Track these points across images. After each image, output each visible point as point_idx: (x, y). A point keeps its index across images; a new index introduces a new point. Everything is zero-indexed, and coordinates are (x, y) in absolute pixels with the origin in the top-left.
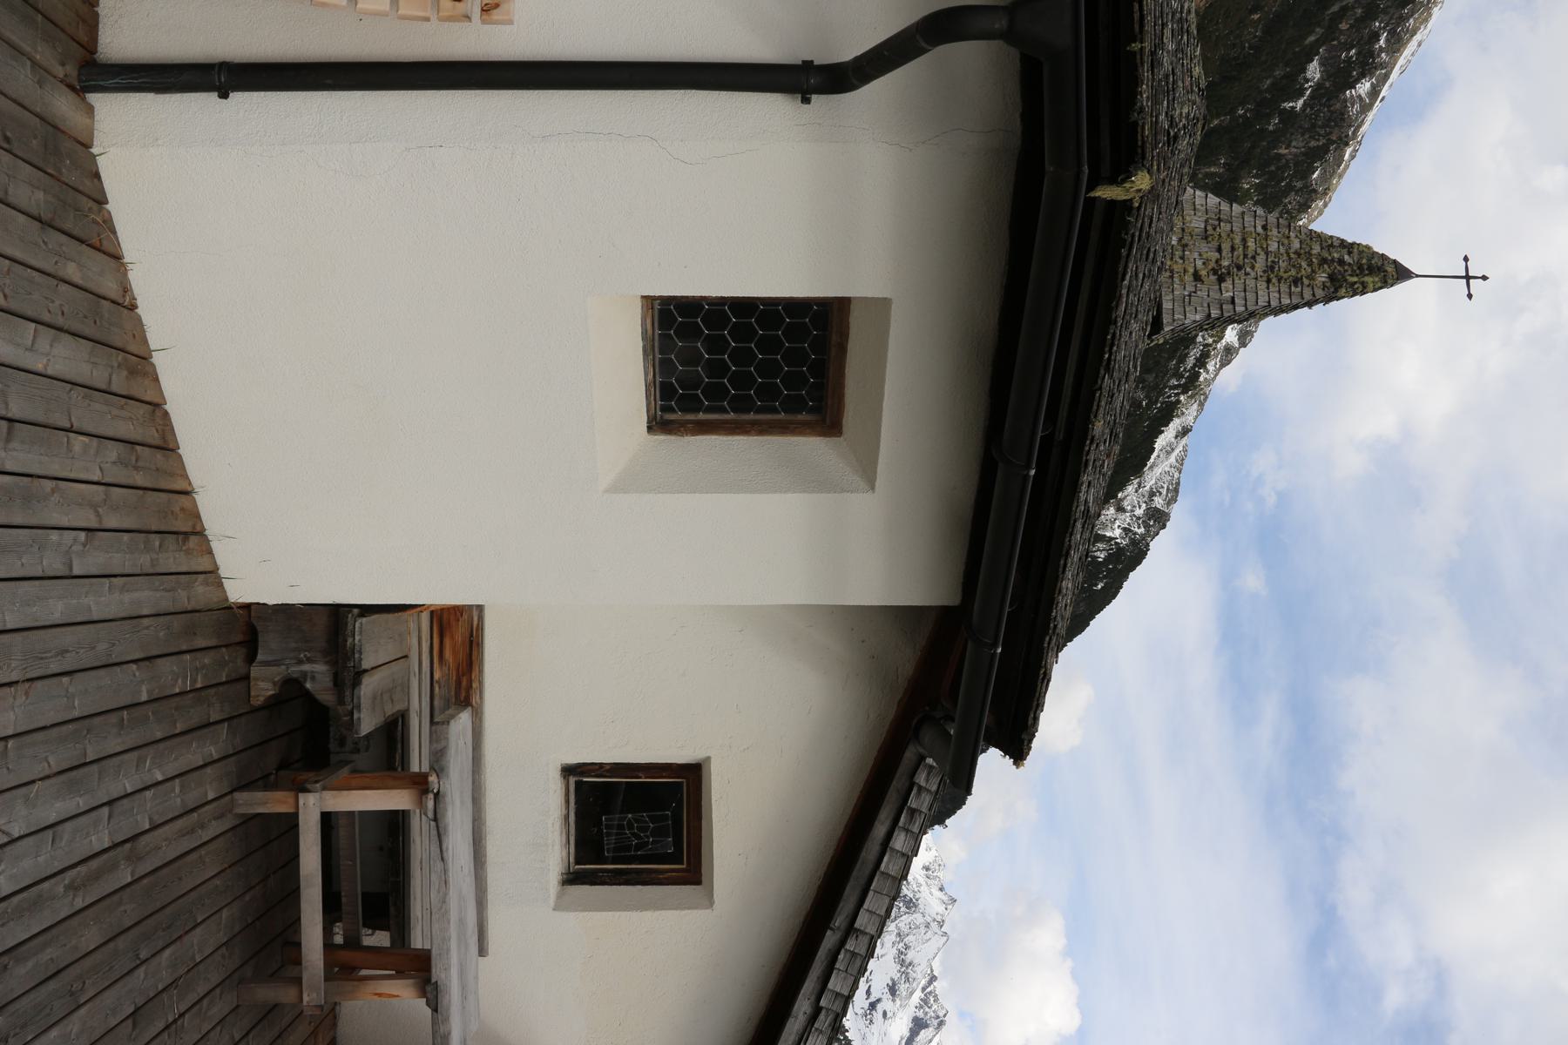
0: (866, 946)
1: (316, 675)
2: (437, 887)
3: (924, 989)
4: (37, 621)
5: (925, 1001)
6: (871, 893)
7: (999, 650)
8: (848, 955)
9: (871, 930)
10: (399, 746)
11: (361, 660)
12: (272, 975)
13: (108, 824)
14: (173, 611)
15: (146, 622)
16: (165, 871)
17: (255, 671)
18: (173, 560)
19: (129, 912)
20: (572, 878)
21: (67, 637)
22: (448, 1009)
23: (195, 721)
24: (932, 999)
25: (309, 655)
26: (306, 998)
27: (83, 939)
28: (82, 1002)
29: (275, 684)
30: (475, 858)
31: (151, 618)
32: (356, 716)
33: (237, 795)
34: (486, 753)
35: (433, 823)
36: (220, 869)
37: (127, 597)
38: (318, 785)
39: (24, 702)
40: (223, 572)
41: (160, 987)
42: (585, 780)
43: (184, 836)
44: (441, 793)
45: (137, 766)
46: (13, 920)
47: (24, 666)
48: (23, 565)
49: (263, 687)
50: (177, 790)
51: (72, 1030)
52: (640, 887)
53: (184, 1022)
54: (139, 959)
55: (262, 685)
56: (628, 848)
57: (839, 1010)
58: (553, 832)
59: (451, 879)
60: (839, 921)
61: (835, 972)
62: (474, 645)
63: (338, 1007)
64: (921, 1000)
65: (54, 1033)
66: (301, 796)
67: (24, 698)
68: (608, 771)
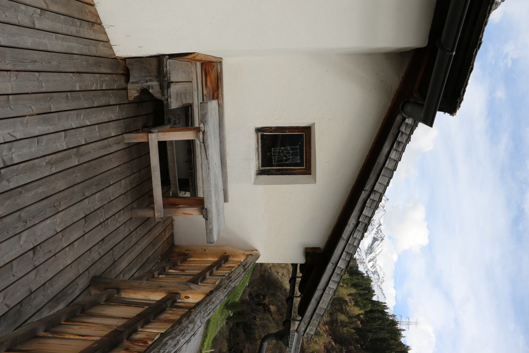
0: (379, 198)
1: (153, 86)
2: (205, 170)
3: (377, 228)
4: (18, 44)
5: (377, 232)
6: (381, 176)
7: (454, 54)
8: (371, 201)
9: (381, 191)
10: (190, 119)
11: (170, 77)
12: (146, 207)
13: (65, 140)
14: (89, 54)
15: (76, 56)
16: (94, 162)
17: (129, 86)
18: (86, 32)
19: (78, 176)
20: (260, 173)
21: (36, 55)
22: (212, 219)
23: (103, 103)
24: (380, 232)
25: (150, 78)
26: (156, 215)
27: (58, 185)
28: (60, 210)
29: (137, 91)
30: (221, 164)
31: (78, 56)
32: (169, 101)
33: (124, 135)
34: (225, 123)
35: (202, 144)
36: (119, 164)
37: (66, 44)
38: (156, 130)
39: (16, 80)
40: (112, 43)
41: (96, 208)
42: (265, 134)
43: (101, 149)
44: (205, 132)
45: (77, 117)
46: (22, 173)
47: (14, 64)
48: (6, 16)
49: (133, 93)
50: (97, 130)
51: (57, 221)
52: (287, 176)
53: (108, 222)
54: (85, 196)
55: (133, 92)
56: (282, 161)
57: (367, 223)
58: (252, 154)
59: (211, 167)
60: (368, 187)
61: (366, 207)
62: (219, 80)
63: (173, 222)
64: (376, 232)
65: (48, 221)
66: (149, 134)
67: (15, 78)
68: (273, 130)
